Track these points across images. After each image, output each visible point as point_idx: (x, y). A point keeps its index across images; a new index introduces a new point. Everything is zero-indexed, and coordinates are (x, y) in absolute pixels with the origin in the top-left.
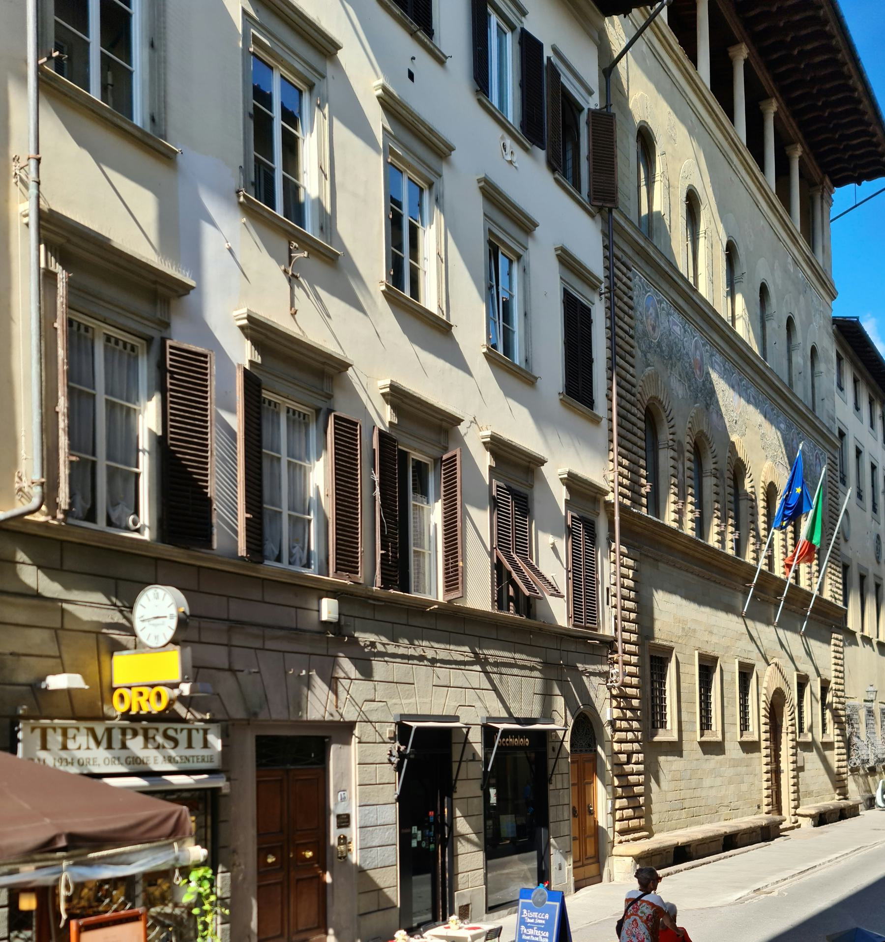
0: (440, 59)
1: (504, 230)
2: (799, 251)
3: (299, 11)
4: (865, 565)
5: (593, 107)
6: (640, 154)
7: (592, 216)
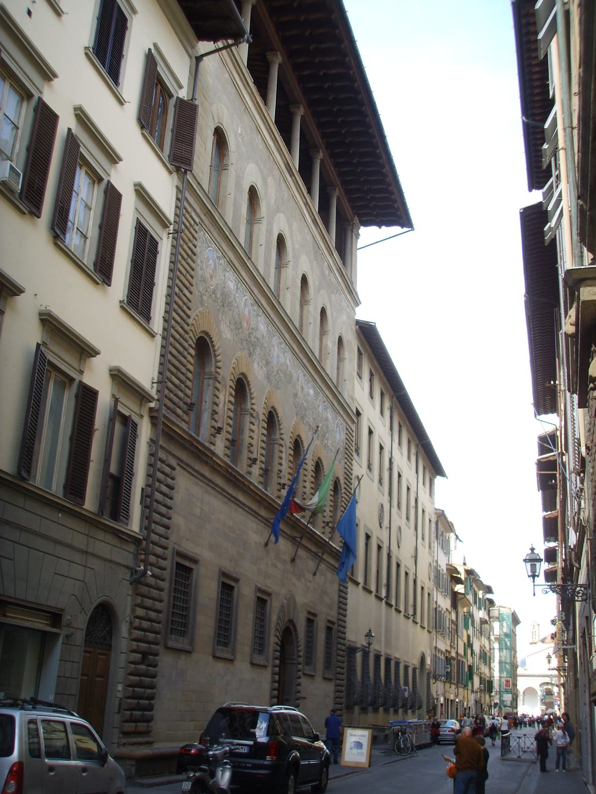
0: (121, 102)
1: (24, 72)
2: (333, 261)
3: (4, 9)
4: (371, 526)
5: (181, 96)
6: (215, 145)
7: (171, 173)
